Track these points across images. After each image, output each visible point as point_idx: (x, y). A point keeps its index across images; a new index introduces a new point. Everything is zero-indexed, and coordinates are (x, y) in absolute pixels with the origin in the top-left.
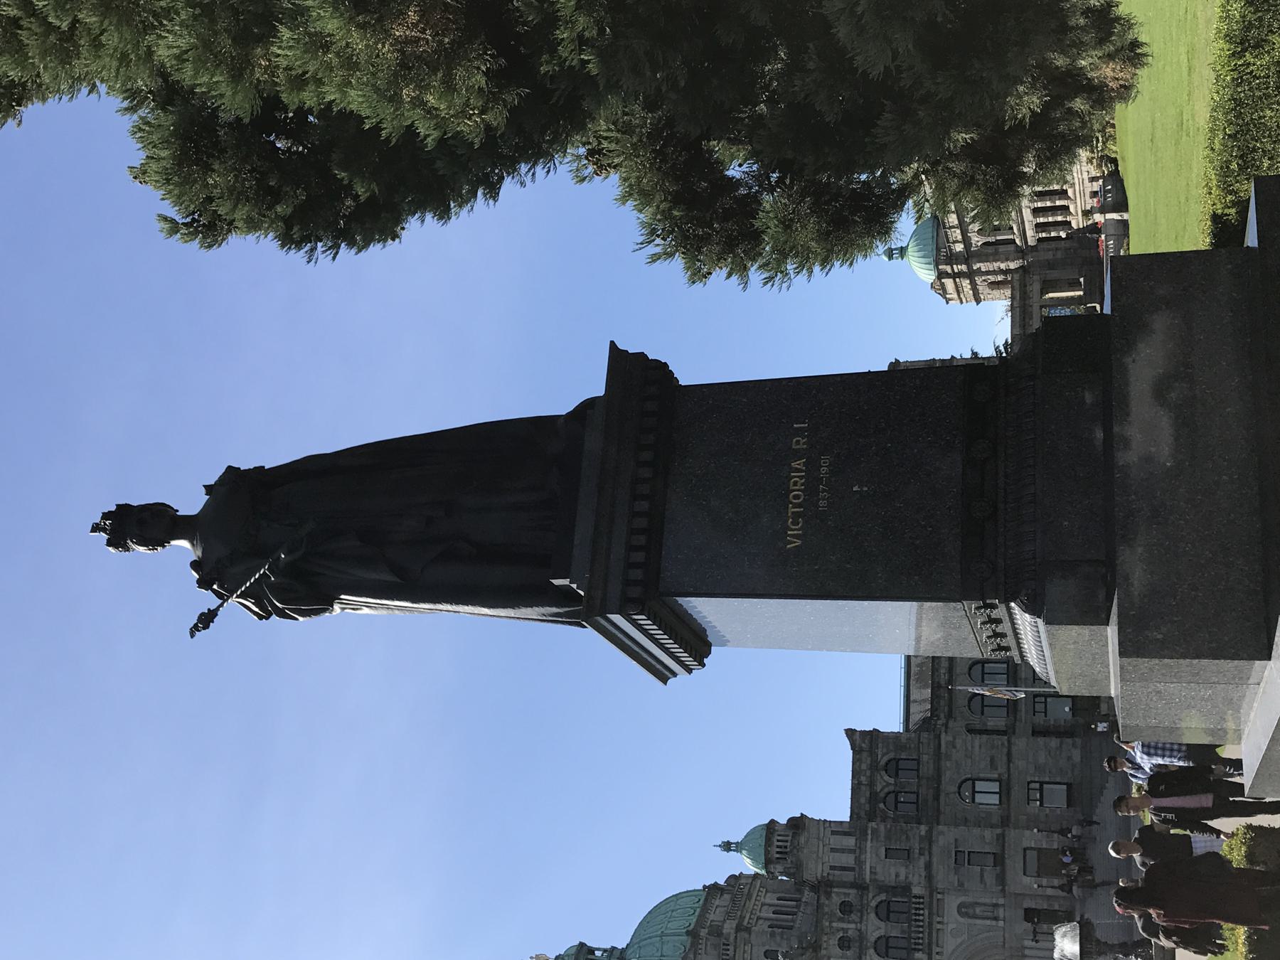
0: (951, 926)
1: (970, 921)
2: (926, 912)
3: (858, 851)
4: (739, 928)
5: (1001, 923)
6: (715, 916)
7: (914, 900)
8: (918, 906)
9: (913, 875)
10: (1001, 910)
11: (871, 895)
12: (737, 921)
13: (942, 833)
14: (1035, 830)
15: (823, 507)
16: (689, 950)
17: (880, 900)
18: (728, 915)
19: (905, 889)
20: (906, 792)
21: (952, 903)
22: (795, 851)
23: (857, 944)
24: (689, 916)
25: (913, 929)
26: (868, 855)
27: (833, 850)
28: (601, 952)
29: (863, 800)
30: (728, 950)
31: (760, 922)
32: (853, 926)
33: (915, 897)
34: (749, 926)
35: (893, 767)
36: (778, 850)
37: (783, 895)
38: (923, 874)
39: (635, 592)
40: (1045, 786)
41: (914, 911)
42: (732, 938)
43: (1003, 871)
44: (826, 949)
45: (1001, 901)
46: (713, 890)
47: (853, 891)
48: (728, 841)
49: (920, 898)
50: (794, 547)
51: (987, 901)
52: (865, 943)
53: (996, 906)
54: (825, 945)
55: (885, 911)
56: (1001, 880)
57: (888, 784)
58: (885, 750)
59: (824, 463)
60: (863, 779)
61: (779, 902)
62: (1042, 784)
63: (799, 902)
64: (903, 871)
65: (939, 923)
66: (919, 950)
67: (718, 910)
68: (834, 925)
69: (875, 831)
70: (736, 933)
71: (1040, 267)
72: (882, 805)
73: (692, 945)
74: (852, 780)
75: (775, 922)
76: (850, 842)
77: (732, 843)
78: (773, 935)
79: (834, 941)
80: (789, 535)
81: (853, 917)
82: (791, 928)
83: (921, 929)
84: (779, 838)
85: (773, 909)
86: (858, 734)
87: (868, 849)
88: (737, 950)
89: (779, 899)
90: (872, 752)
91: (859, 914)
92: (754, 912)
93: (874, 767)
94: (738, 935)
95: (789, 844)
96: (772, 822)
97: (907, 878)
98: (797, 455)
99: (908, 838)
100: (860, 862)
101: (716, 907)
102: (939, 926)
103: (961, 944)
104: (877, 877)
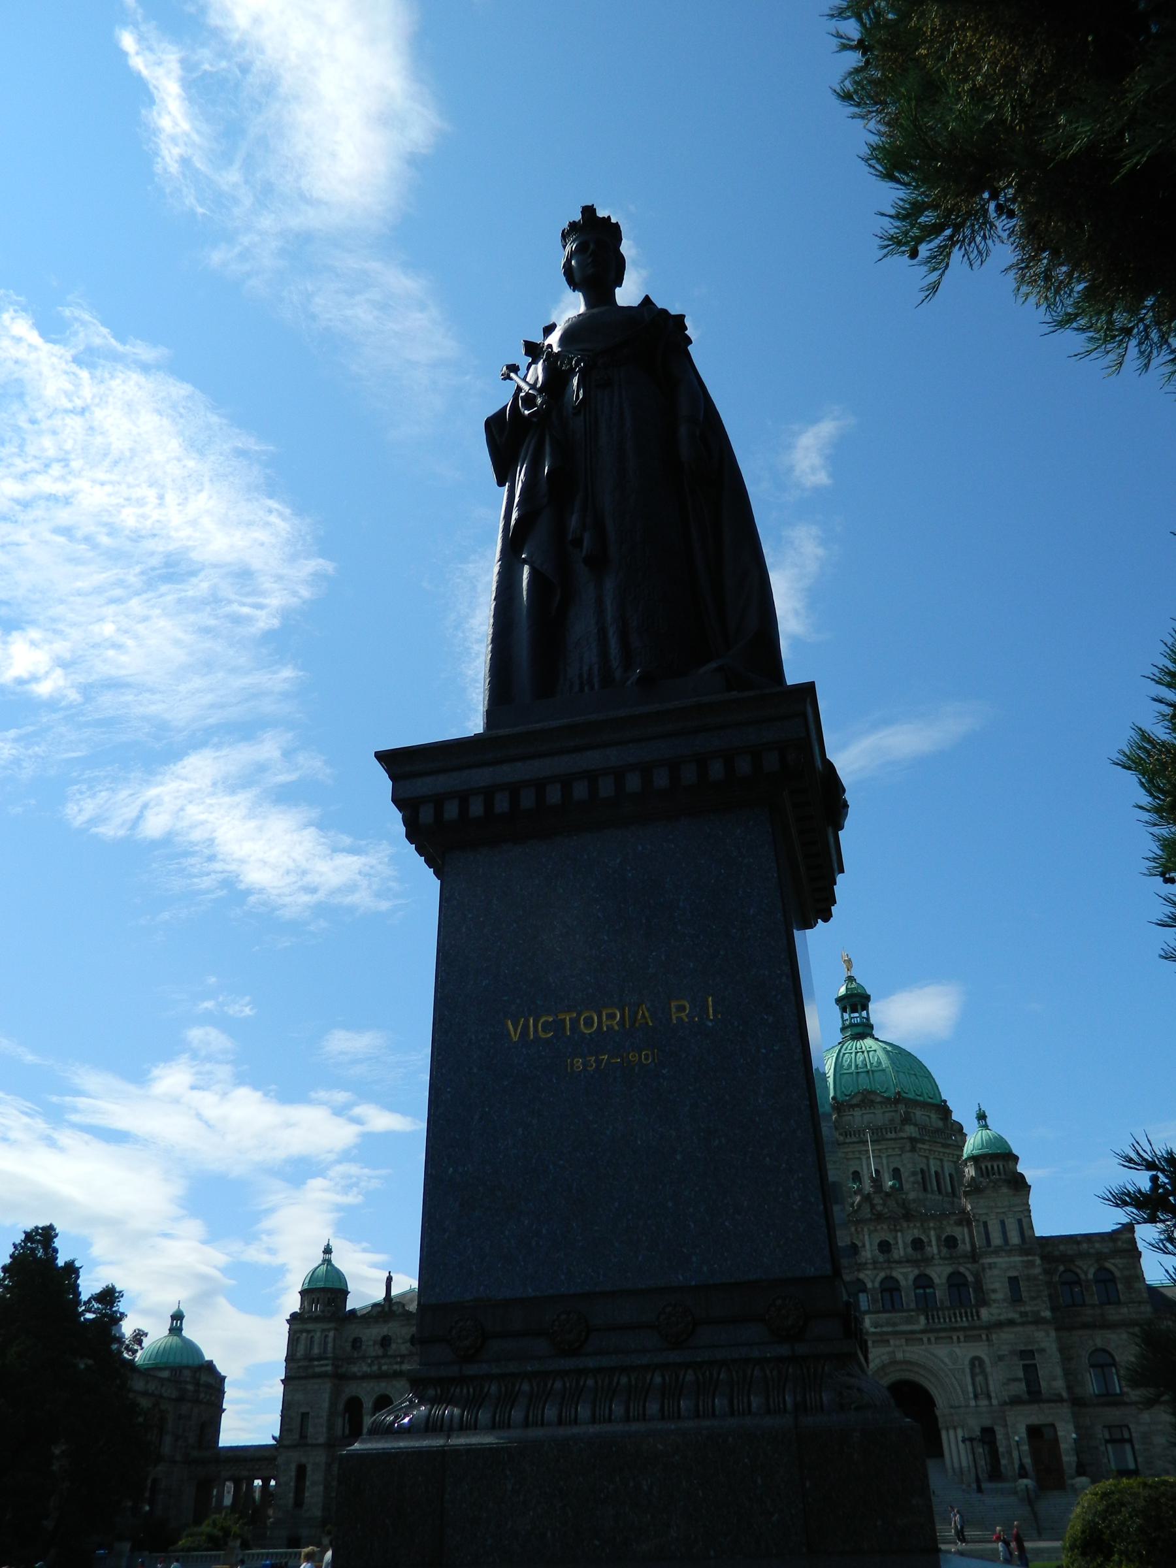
0: (957, 1350)
1: (968, 1370)
2: (966, 1324)
3: (1008, 1248)
4: (912, 1140)
5: (973, 1403)
6: (919, 1114)
7: (974, 1311)
8: (969, 1314)
9: (998, 1307)
10: (985, 1402)
11: (969, 1266)
12: (918, 1137)
13: (1048, 1335)
15: (572, 1064)
16: (882, 1096)
18: (922, 1128)
19: (983, 1302)
20: (1082, 1291)
21: (980, 1350)
22: (992, 1184)
23: (919, 1257)
24: (915, 1091)
25: (946, 1313)
26: (1007, 1259)
27: (1003, 1223)
28: (866, 1016)
29: (1062, 1248)
30: (891, 1133)
31: (924, 1160)
32: (935, 1251)
33: (978, 1312)
34: (918, 1150)
35: (1106, 1279)
36: (989, 1167)
37: (956, 1179)
38: (1002, 1317)
41: (963, 1311)
42: (902, 1135)
44: (908, 1227)
45: (995, 1402)
46: (944, 1110)
47: (968, 1247)
48: (986, 1117)
50: (508, 1031)
51: (992, 1388)
52: (923, 1264)
53: (989, 1397)
54: (912, 1225)
55: (956, 1282)
56: (1015, 1401)
57: (1086, 1273)
58: (1120, 1266)
59: (646, 1055)
60: (1085, 1246)
61: (933, 1173)
63: (937, 1193)
64: (999, 1296)
65: (958, 1338)
66: (927, 1319)
67: (927, 1118)
68: (932, 1233)
69: (1031, 1264)
70: (907, 1138)
72: (1062, 1268)
73: (888, 1099)
74: (1081, 1235)
75: (927, 1174)
76: (1015, 1239)
77: (985, 1121)
78: (914, 1174)
79: (916, 1233)
80: (527, 1021)
81: (944, 1251)
82: (925, 1189)
83: (947, 1320)
84: (1001, 1167)
85: (939, 1170)
86: (1130, 1235)
87: (1012, 1259)
88: (893, 1142)
89: (950, 1175)
90: (1116, 1253)
91: (948, 1256)
92: (932, 1153)
93: (1100, 1257)
94: (905, 1141)
95: (998, 1177)
96: (1016, 1159)
97: (994, 1301)
99: (1033, 1299)
100: (997, 1251)
101: (928, 1116)
102: (955, 1338)
103: (942, 1361)
104: (988, 1270)
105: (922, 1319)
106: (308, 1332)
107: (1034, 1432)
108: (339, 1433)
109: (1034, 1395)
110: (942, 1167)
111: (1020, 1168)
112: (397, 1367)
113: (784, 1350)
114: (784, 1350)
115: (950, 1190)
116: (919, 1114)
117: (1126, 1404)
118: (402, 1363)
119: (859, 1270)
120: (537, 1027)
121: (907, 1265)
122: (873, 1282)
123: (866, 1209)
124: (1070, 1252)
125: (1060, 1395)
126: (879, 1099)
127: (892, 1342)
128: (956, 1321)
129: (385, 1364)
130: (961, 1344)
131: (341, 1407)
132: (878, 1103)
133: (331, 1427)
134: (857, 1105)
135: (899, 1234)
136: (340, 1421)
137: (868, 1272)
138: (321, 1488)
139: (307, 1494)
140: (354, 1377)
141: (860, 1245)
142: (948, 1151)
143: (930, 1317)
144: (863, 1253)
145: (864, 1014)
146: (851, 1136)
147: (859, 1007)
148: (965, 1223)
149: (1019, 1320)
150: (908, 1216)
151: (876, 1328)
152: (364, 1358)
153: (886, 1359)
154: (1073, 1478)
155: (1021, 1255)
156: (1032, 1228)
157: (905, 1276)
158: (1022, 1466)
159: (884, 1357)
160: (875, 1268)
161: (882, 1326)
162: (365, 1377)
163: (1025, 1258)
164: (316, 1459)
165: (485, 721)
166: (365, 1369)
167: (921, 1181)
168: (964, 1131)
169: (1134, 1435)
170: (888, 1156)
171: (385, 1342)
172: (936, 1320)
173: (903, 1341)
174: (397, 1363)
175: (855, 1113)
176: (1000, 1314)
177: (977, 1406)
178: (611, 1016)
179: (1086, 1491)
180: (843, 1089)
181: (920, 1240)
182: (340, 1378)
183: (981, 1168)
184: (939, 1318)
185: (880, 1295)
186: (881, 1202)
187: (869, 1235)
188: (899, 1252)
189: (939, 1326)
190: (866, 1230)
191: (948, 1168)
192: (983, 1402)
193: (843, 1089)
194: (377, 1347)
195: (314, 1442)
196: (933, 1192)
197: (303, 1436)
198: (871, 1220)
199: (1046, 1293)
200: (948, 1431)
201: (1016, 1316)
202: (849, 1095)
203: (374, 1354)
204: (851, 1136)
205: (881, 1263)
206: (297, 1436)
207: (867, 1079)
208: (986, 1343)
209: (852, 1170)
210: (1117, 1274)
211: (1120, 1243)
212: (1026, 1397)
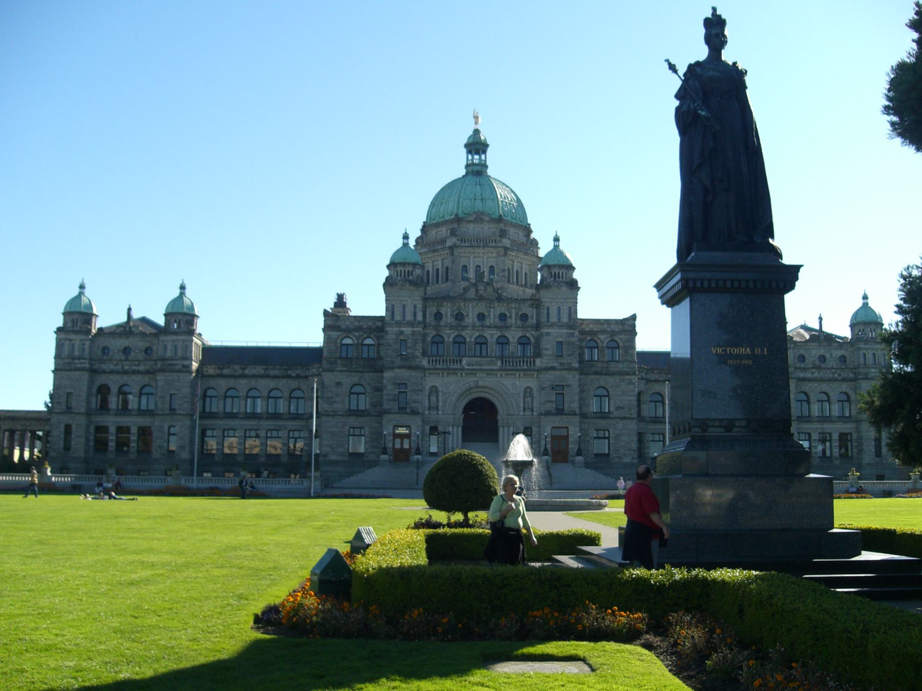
1: (522, 395)
2: (525, 367)
4: (506, 249)
5: (522, 413)
10: (530, 413)
11: (533, 333)
14: (579, 434)
18: (513, 242)
19: (538, 354)
21: (533, 383)
26: (557, 331)
27: (559, 308)
31: (511, 262)
32: (514, 321)
33: (534, 361)
35: (613, 346)
36: (557, 273)
39: (691, 284)
40: (607, 441)
42: (500, 244)
45: (535, 413)
46: (528, 230)
47: (534, 321)
49: (534, 363)
55: (523, 342)
56: (548, 413)
57: (602, 342)
58: (623, 340)
62: (608, 438)
65: (520, 375)
66: (502, 363)
67: (516, 234)
69: (572, 335)
72: (589, 338)
75: (511, 272)
76: (565, 319)
79: (503, 310)
81: (519, 323)
83: (515, 364)
84: (564, 274)
87: (561, 331)
89: (526, 274)
90: (623, 331)
93: (613, 333)
97: (546, 355)
98: (752, 350)
99: (569, 355)
100: (552, 325)
103: (507, 388)
105: (499, 363)
106: (70, 340)
108: (94, 406)
109: (560, 412)
110: (521, 268)
111: (575, 275)
112: (135, 368)
115: (524, 283)
116: (512, 231)
117: (610, 418)
118: (138, 365)
119: (462, 330)
121: (495, 329)
122: (471, 338)
123: (473, 291)
124: (595, 329)
125: (574, 411)
126: (487, 219)
127: (478, 375)
128: (520, 365)
129: (126, 365)
130: (521, 379)
131: (94, 390)
132: (486, 221)
133: (88, 402)
134: (472, 222)
135: (492, 310)
136: (93, 399)
137: (468, 332)
138: (83, 440)
139: (73, 443)
140: (104, 372)
141: (465, 314)
142: (526, 257)
143: (504, 362)
144: (467, 320)
145: (483, 157)
146: (465, 242)
147: (481, 152)
148: (534, 306)
149: (559, 368)
150: (499, 299)
151: (469, 366)
152: (111, 360)
153: (472, 385)
154: (573, 456)
155: (567, 329)
156: (576, 313)
157: (492, 335)
158: (546, 449)
159: (471, 384)
160: (473, 330)
161: (473, 365)
162: (112, 372)
163: (568, 331)
164: (78, 423)
166: (112, 367)
167: (507, 275)
168: (539, 246)
169: (611, 435)
170: (488, 257)
171: (126, 351)
172: (508, 364)
173: (485, 375)
174: (135, 365)
175: (469, 227)
176: (547, 363)
177: (524, 415)
178: (740, 350)
180: (464, 209)
181: (505, 315)
182: (93, 372)
183: (551, 273)
184: (509, 363)
185: (473, 347)
186: (483, 288)
187: (472, 309)
188: (492, 319)
189: (508, 368)
190: (471, 305)
191: (525, 269)
192: (528, 413)
193: (464, 209)
194: (121, 354)
195: (77, 411)
196: (513, 283)
197: (171, 409)
198: (474, 299)
199: (578, 353)
200: (453, 427)
201: (556, 365)
202: (467, 214)
203: (118, 358)
204: (465, 242)
205: (477, 327)
206: (64, 407)
207: (481, 204)
208: (536, 379)
209: (462, 264)
210: (621, 344)
211: (626, 326)
212: (554, 411)
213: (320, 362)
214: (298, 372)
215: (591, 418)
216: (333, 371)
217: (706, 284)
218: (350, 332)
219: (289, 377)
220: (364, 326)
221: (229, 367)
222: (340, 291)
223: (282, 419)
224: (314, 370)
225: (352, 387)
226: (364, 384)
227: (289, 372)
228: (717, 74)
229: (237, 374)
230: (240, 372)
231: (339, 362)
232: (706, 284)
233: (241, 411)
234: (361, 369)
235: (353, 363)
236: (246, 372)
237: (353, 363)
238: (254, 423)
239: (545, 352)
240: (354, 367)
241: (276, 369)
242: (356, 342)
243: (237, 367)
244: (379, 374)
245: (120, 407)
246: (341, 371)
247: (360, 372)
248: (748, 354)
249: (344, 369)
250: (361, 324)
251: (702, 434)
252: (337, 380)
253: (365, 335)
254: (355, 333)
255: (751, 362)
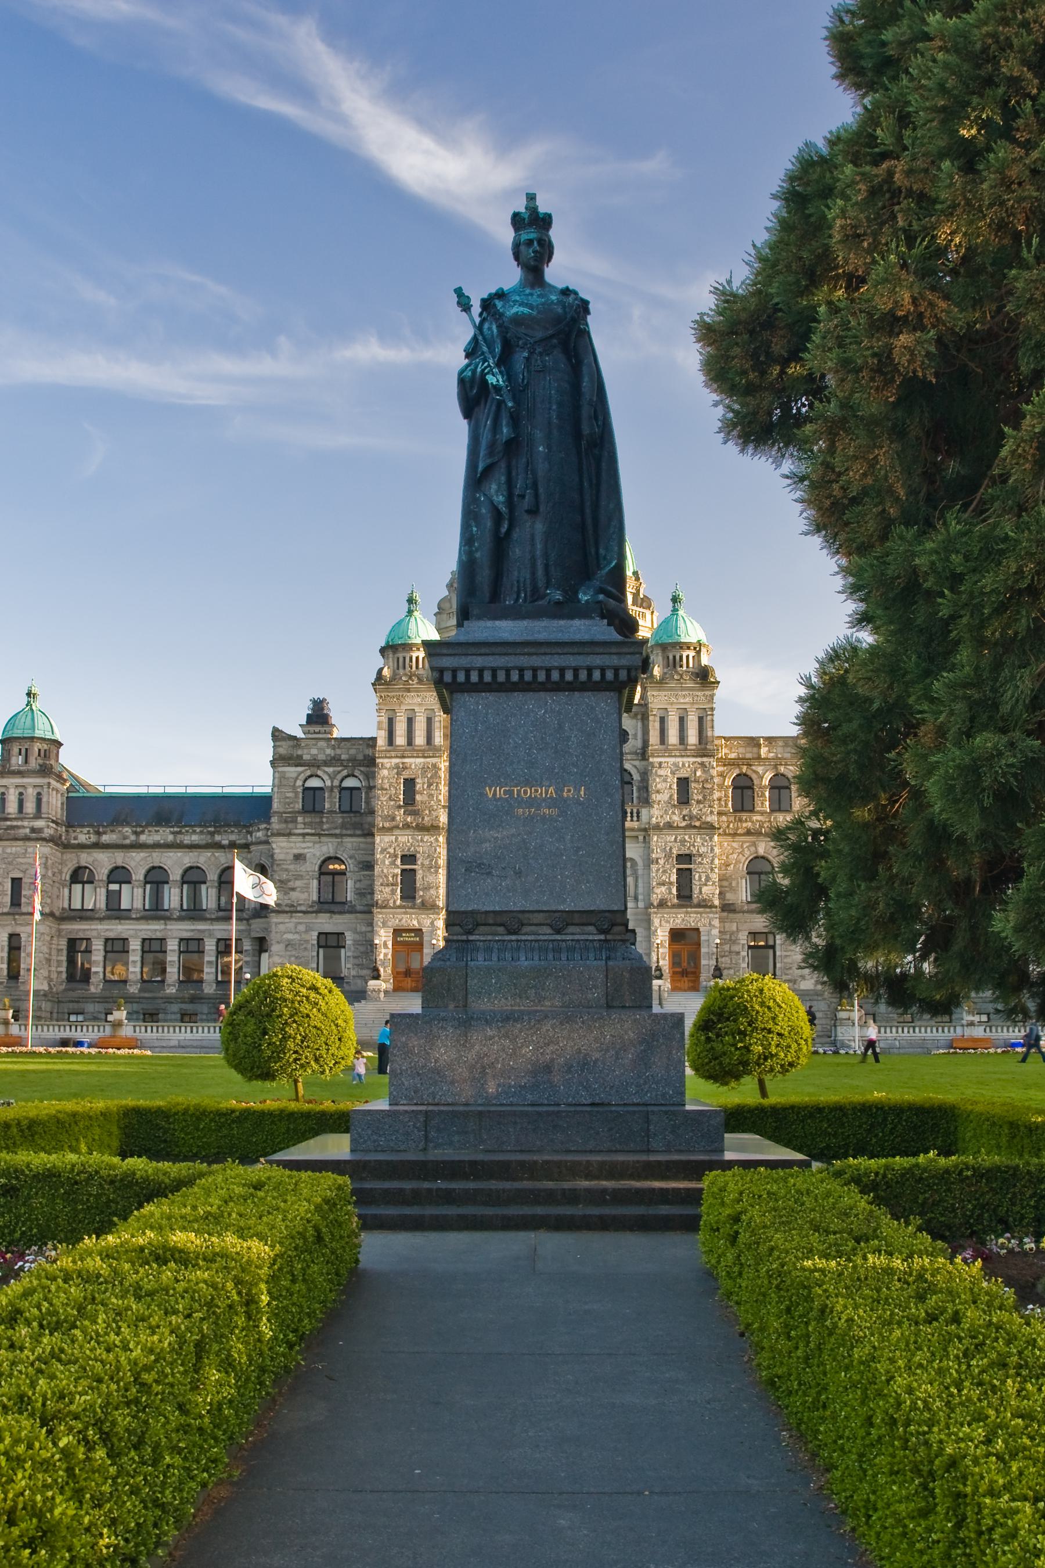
11: (637, 763)
14: (718, 941)
17: (632, 773)
33: (638, 813)
39: (448, 678)
40: (771, 952)
43: (71, 961)
47: (639, 744)
49: (638, 817)
62: (773, 947)
64: (664, 797)
71: (277, 976)
98: (559, 790)
100: (668, 752)
107: (677, 935)
113: (602, 937)
114: (602, 937)
120: (500, 792)
148: (639, 717)
165: (779, 1106)
178: (536, 791)
179: (950, 904)
213: (267, 819)
214: (233, 837)
215: (744, 912)
216: (290, 834)
217: (474, 677)
218: (318, 767)
219: (218, 846)
220: (343, 757)
221: (112, 831)
222: (318, 695)
223: (206, 919)
224: (260, 834)
225: (324, 862)
226: (344, 856)
227: (217, 838)
228: (526, 310)
229: (127, 842)
230: (133, 838)
231: (300, 819)
232: (474, 677)
233: (135, 906)
234: (338, 831)
235: (324, 820)
236: (143, 838)
237: (324, 820)
238: (157, 927)
239: (654, 797)
240: (325, 827)
241: (194, 832)
242: (328, 783)
243: (127, 830)
244: (369, 840)
245: (147, 907)
246: (304, 835)
247: (335, 836)
248: (551, 797)
249: (309, 831)
250: (338, 751)
251: (464, 938)
252: (296, 851)
253: (345, 773)
254: (326, 769)
255: (555, 812)
